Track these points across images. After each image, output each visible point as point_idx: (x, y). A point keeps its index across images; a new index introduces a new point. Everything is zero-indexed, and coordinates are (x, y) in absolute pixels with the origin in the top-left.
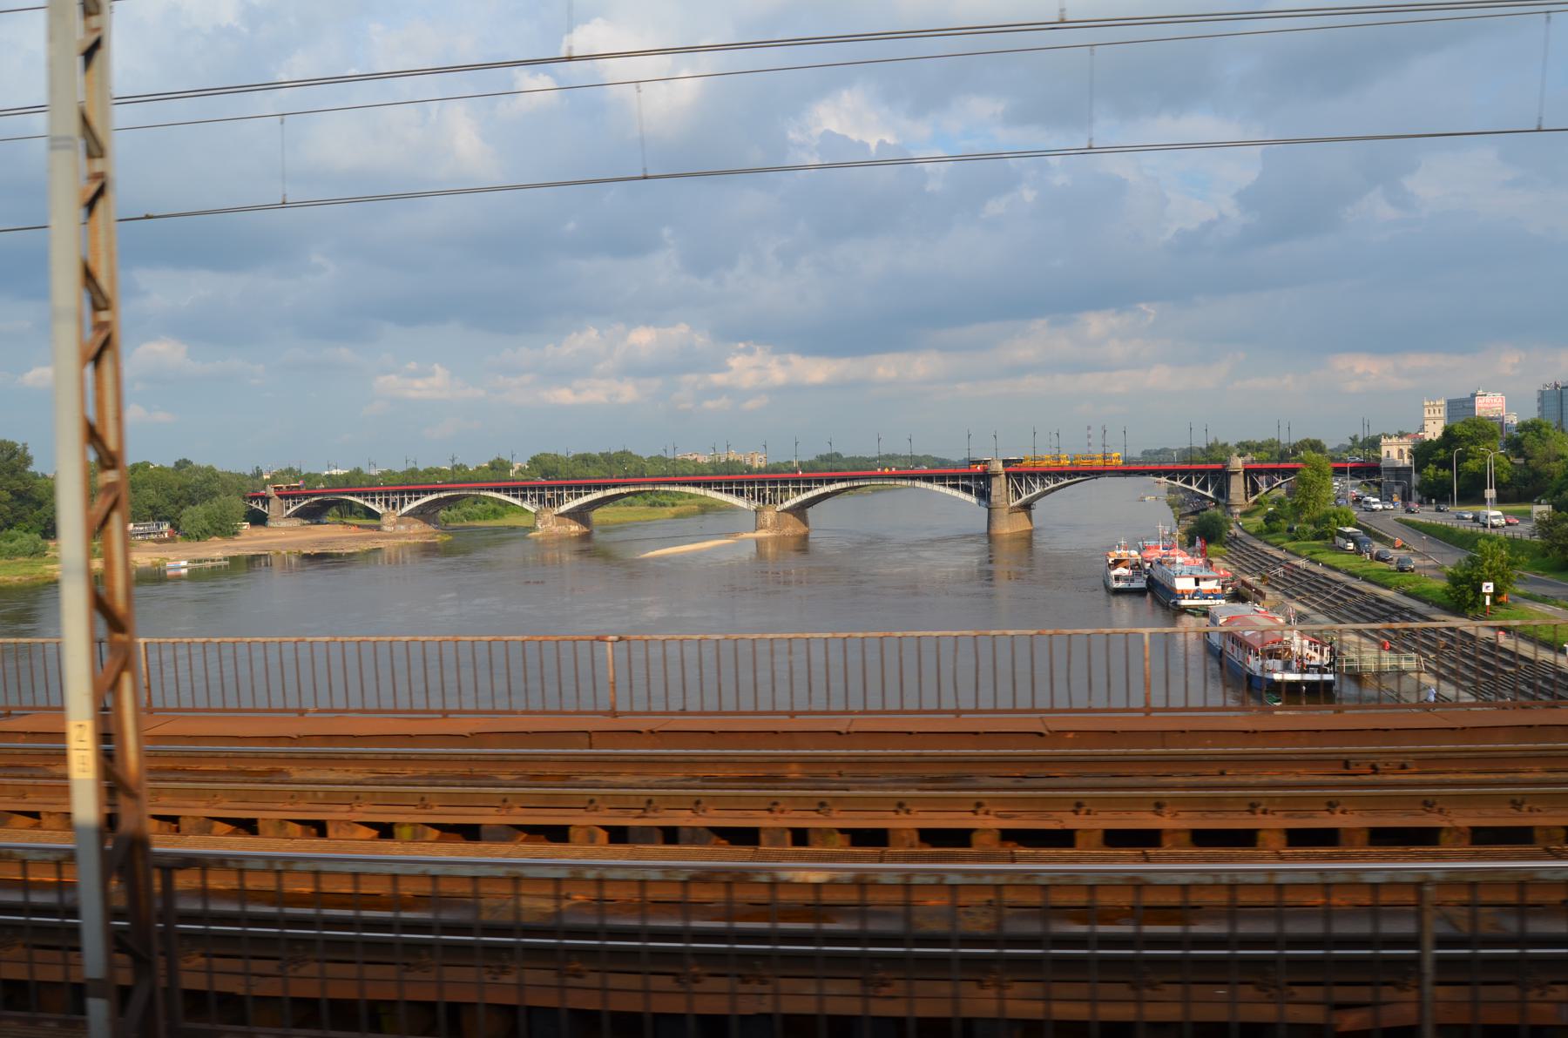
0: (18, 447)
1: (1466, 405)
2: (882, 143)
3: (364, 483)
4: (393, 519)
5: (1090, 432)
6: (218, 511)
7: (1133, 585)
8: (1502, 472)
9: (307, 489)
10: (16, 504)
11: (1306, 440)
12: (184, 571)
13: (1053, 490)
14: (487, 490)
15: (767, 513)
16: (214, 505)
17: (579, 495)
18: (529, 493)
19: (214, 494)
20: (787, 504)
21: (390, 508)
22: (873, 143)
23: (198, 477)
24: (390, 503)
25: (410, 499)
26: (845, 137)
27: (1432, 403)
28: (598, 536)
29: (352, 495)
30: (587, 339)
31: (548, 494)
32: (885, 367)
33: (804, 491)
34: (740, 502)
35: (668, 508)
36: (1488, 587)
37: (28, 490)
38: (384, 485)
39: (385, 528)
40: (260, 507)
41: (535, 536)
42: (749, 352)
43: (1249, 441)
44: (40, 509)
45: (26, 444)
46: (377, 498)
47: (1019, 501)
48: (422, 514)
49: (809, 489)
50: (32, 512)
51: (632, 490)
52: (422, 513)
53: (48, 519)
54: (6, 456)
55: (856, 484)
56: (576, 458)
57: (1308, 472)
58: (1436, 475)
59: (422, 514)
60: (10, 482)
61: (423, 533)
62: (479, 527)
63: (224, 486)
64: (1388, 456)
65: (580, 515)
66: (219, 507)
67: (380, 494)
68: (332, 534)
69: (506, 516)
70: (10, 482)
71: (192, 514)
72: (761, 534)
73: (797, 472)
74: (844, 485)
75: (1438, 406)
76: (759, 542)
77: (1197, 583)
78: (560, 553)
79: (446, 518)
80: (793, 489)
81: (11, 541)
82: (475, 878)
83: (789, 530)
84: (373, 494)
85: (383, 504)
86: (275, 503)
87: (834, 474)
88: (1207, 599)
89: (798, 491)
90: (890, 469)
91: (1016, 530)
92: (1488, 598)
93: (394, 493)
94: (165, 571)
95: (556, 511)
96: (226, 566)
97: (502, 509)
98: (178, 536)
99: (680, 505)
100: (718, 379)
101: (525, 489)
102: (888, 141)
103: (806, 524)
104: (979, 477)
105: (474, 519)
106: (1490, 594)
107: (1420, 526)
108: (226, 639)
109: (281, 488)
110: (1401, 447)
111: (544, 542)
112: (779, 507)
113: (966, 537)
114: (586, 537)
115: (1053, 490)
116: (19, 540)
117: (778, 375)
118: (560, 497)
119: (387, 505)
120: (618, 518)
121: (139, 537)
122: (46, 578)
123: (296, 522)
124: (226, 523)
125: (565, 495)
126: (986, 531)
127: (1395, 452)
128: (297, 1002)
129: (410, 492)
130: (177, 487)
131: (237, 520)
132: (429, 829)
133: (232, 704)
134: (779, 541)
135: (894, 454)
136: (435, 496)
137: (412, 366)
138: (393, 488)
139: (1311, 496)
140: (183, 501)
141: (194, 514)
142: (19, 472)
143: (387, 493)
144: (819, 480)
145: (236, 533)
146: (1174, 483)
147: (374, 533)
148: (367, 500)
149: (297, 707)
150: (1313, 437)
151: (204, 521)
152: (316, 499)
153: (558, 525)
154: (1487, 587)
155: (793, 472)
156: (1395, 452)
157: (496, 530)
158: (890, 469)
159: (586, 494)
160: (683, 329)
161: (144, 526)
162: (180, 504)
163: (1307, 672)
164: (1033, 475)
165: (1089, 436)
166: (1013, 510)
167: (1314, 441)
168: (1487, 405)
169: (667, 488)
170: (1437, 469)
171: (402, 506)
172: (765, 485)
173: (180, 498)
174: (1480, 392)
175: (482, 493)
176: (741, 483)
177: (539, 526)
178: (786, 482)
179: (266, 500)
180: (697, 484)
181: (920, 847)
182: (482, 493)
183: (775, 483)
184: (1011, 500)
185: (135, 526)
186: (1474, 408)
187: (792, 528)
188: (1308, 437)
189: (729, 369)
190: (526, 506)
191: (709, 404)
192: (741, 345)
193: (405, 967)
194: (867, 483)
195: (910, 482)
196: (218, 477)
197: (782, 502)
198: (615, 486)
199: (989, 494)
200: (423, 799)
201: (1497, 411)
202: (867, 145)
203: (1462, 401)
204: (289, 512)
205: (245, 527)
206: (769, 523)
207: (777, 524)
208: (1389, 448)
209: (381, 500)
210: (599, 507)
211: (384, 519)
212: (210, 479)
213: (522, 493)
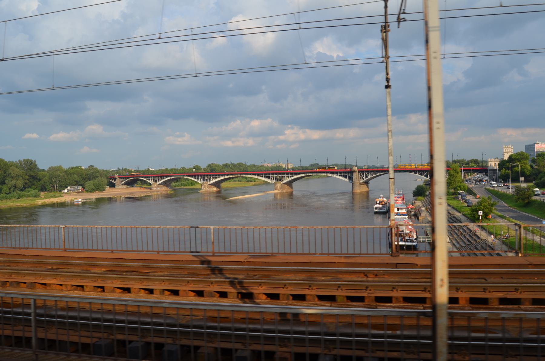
0: (33, 161)
1: (532, 147)
2: (338, 56)
3: (149, 173)
4: (155, 186)
5: (410, 156)
6: (98, 183)
7: (381, 211)
8: (527, 171)
10: (31, 180)
11: (473, 159)
13: (375, 177)
14: (186, 176)
16: (96, 181)
17: (216, 178)
18: (200, 177)
19: (97, 177)
20: (285, 181)
21: (155, 182)
22: (335, 55)
23: (91, 171)
24: (155, 180)
25: (161, 179)
26: (325, 54)
27: (506, 147)
28: (223, 192)
30: (237, 124)
31: (206, 178)
32: (339, 134)
33: (291, 177)
34: (269, 181)
35: (252, 182)
36: (481, 213)
37: (36, 175)
38: (237, 172)
39: (153, 189)
40: (113, 181)
41: (201, 192)
42: (292, 128)
43: (59, 169)
44: (40, 181)
45: (35, 160)
46: (151, 179)
47: (363, 181)
48: (165, 184)
49: (292, 176)
50: (37, 183)
51: (233, 176)
52: (165, 184)
53: (42, 185)
54: (29, 164)
55: (308, 175)
56: (223, 165)
57: (452, 171)
58: (505, 172)
59: (165, 184)
60: (30, 173)
61: (165, 190)
62: (186, 189)
63: (100, 174)
64: (491, 165)
65: (217, 185)
66: (98, 181)
67: (152, 177)
68: (137, 191)
69: (196, 185)
70: (30, 173)
71: (89, 183)
72: (275, 191)
74: (303, 175)
75: (508, 148)
76: (275, 195)
77: (398, 210)
78: (210, 197)
79: (175, 185)
80: (287, 176)
81: (28, 192)
82: (102, 304)
83: (285, 190)
84: (149, 177)
85: (202, 180)
87: (300, 171)
88: (400, 216)
89: (288, 177)
90: (316, 170)
91: (362, 191)
92: (480, 217)
93: (156, 177)
94: (74, 203)
95: (208, 183)
96: (94, 201)
97: (193, 183)
98: (84, 191)
99: (257, 181)
100: (282, 137)
101: (198, 176)
103: (292, 188)
104: (349, 172)
105: (185, 186)
106: (481, 215)
107: (490, 190)
108: (99, 226)
110: (495, 162)
111: (205, 194)
112: (282, 183)
113: (344, 193)
114: (219, 192)
115: (375, 177)
116: (31, 192)
117: (302, 136)
118: (210, 179)
119: (154, 181)
121: (72, 191)
122: (35, 204)
123: (125, 186)
124: (100, 187)
125: (211, 178)
126: (351, 191)
127: (493, 164)
129: (161, 177)
130: (85, 175)
131: (104, 186)
132: (190, 292)
134: (282, 194)
135: (337, 164)
136: (169, 178)
137: (178, 133)
138: (156, 175)
139: (453, 180)
140: (87, 179)
141: (90, 184)
142: (32, 169)
144: (295, 173)
145: (104, 190)
146: (416, 174)
147: (149, 190)
148: (147, 179)
150: (475, 158)
151: (93, 186)
152: (131, 179)
153: (209, 188)
154: (480, 213)
156: (493, 164)
157: (192, 189)
158: (316, 170)
159: (218, 178)
160: (269, 120)
161: (73, 187)
162: (86, 180)
163: (407, 242)
164: (368, 172)
165: (410, 158)
166: (361, 184)
167: (476, 160)
168: (539, 147)
169: (245, 176)
170: (506, 170)
171: (210, 181)
172: (277, 175)
173: (86, 178)
174: (537, 142)
175: (184, 177)
176: (269, 174)
177: (203, 188)
178: (284, 174)
179: (115, 179)
180: (255, 174)
181: (404, 303)
182: (184, 177)
183: (280, 174)
184: (360, 180)
185: (70, 187)
186: (535, 148)
187: (287, 189)
188: (473, 158)
189: (285, 134)
190: (199, 181)
191: (278, 146)
192: (289, 126)
194: (311, 174)
195: (326, 174)
196: (98, 171)
197: (361, 181)
198: (228, 175)
199: (353, 178)
201: (543, 149)
202: (333, 57)
203: (531, 145)
204: (122, 183)
205: (108, 188)
206: (278, 188)
207: (281, 188)
208: (491, 163)
209: (152, 179)
210: (223, 182)
211: (153, 186)
212: (96, 172)
213: (200, 177)
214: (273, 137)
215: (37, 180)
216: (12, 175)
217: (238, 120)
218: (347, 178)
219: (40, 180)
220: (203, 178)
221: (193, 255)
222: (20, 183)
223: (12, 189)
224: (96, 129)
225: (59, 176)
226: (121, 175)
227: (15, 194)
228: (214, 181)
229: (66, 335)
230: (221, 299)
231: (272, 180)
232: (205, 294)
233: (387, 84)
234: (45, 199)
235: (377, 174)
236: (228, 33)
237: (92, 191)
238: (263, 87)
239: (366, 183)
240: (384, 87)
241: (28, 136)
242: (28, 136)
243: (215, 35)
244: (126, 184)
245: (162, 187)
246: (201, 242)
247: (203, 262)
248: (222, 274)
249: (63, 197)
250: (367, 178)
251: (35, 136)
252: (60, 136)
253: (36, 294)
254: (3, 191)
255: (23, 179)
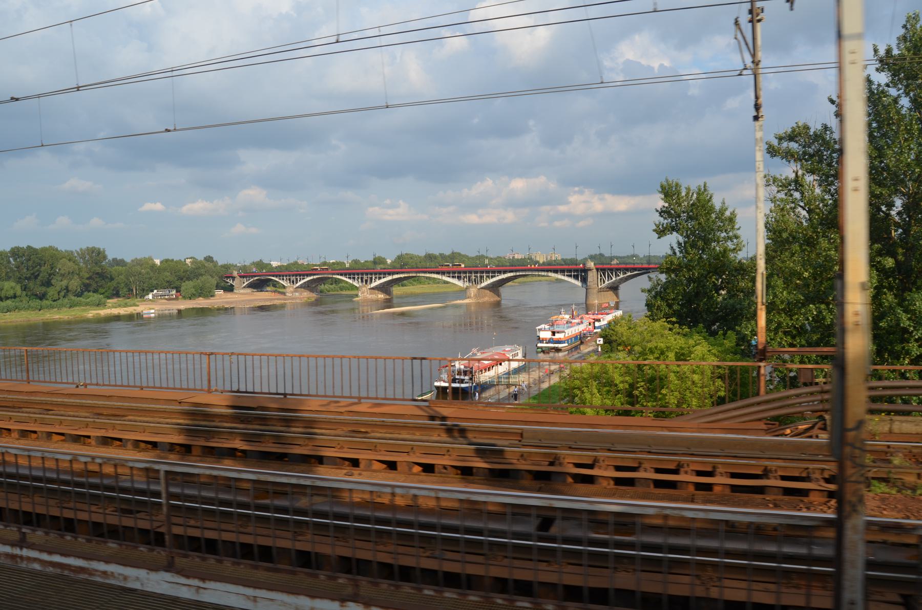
2: (661, 66)
4: (291, 289)
9: (332, 270)
12: (153, 315)
15: (471, 289)
18: (462, 275)
20: (483, 285)
21: (364, 283)
22: (656, 65)
26: (639, 63)
29: (273, 276)
30: (487, 185)
31: (365, 277)
37: (104, 273)
39: (287, 294)
40: (231, 282)
42: (581, 193)
46: (285, 278)
48: (306, 286)
49: (495, 276)
51: (406, 275)
55: (518, 274)
59: (306, 286)
67: (286, 276)
68: (265, 297)
71: (187, 285)
73: (487, 267)
77: (554, 333)
84: (283, 276)
85: (360, 280)
86: (238, 280)
90: (531, 266)
93: (293, 276)
94: (142, 315)
100: (562, 208)
102: (666, 64)
103: (499, 295)
109: (449, 265)
112: (479, 287)
119: (362, 281)
120: (432, 291)
123: (249, 290)
128: (566, 587)
129: (300, 275)
133: (171, 386)
136: (312, 278)
137: (388, 202)
141: (187, 286)
143: (290, 276)
149: (283, 392)
152: (257, 278)
153: (371, 294)
155: (484, 266)
158: (531, 266)
159: (384, 277)
160: (542, 179)
166: (601, 290)
171: (296, 283)
176: (459, 273)
178: (482, 272)
180: (438, 273)
189: (570, 203)
191: (557, 224)
192: (577, 189)
193: (336, 539)
200: (448, 451)
202: (653, 68)
206: (472, 295)
209: (358, 278)
211: (288, 290)
214: (547, 208)
215: (107, 280)
216: (62, 272)
217: (488, 179)
218: (578, 280)
219: (112, 279)
220: (362, 279)
221: (418, 407)
222: (75, 284)
223: (62, 294)
224: (254, 195)
225: (140, 273)
226: (248, 271)
227: (66, 300)
228: (378, 282)
229: (370, 550)
230: (424, 476)
231: (464, 282)
232: (436, 470)
233: (755, 114)
234: (113, 308)
235: (626, 273)
236: (469, 28)
237: (191, 297)
238: (531, 123)
239: (614, 288)
240: (751, 119)
241: (148, 206)
242: (148, 206)
243: (445, 32)
244: (250, 286)
245: (302, 292)
246: (188, 379)
247: (432, 418)
248: (465, 437)
249: (138, 306)
250: (610, 281)
251: (158, 206)
252: (198, 206)
253: (466, 487)
254: (48, 296)
255: (81, 278)
